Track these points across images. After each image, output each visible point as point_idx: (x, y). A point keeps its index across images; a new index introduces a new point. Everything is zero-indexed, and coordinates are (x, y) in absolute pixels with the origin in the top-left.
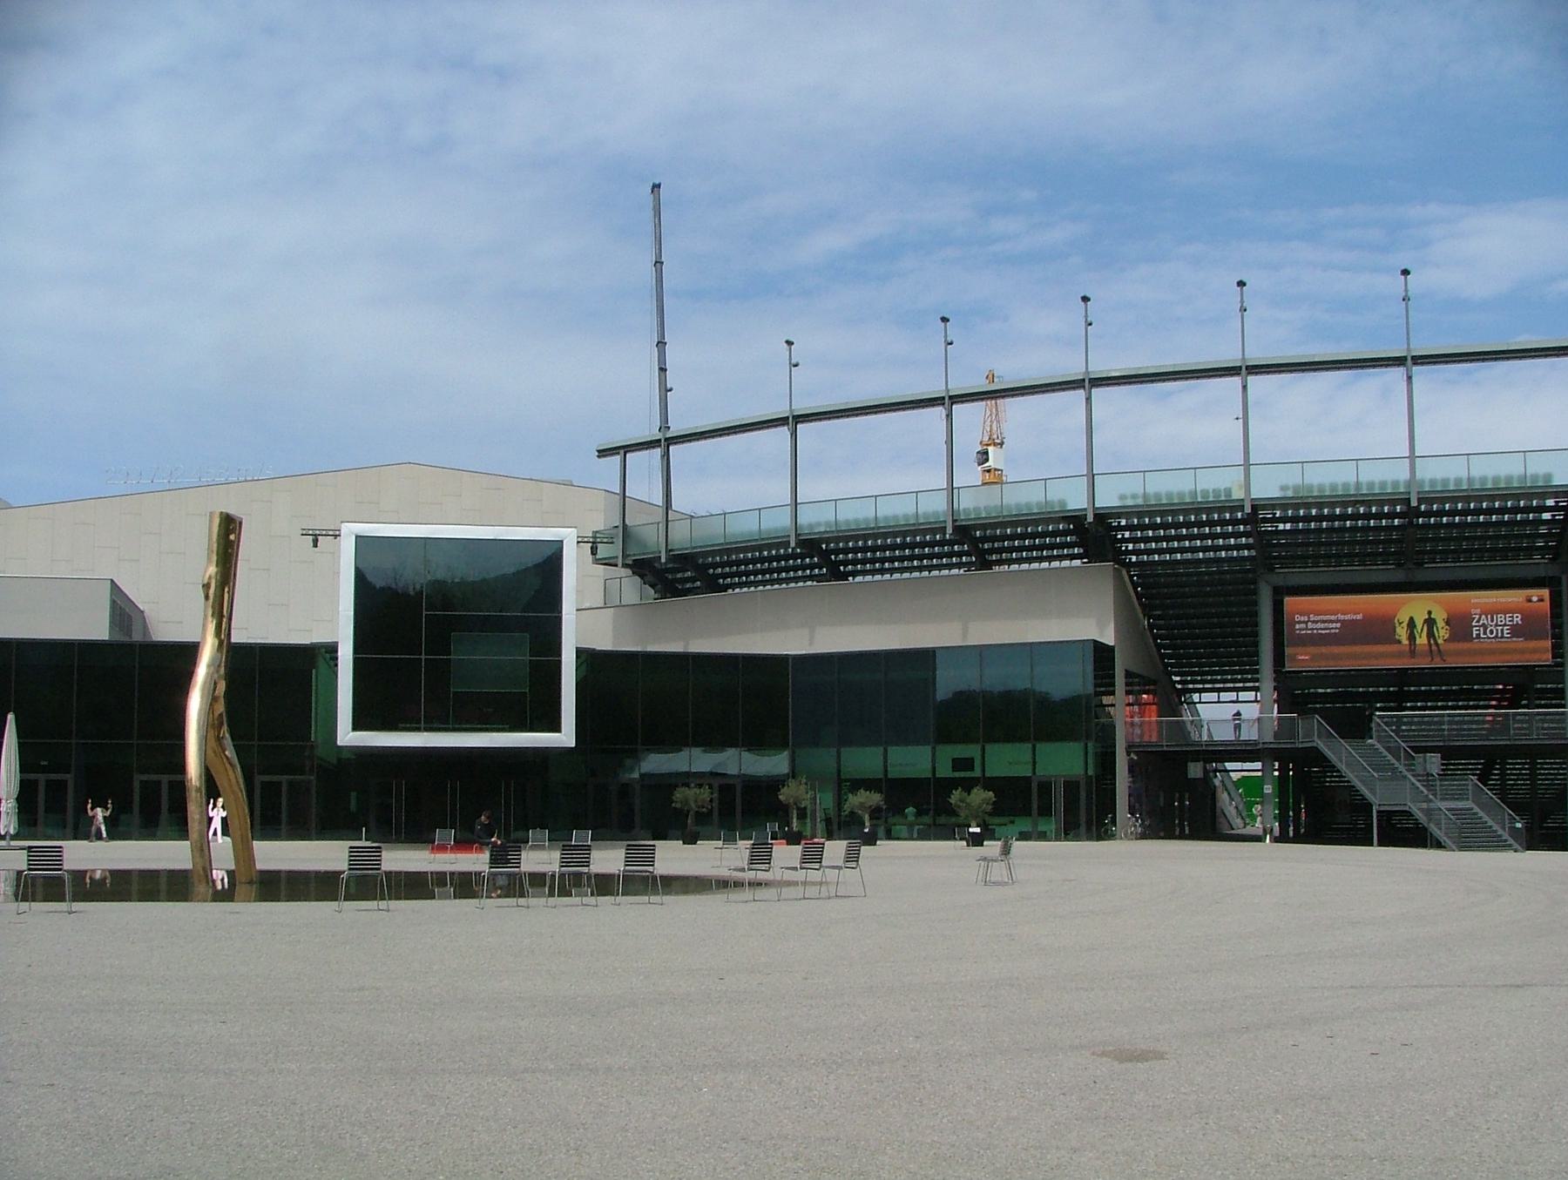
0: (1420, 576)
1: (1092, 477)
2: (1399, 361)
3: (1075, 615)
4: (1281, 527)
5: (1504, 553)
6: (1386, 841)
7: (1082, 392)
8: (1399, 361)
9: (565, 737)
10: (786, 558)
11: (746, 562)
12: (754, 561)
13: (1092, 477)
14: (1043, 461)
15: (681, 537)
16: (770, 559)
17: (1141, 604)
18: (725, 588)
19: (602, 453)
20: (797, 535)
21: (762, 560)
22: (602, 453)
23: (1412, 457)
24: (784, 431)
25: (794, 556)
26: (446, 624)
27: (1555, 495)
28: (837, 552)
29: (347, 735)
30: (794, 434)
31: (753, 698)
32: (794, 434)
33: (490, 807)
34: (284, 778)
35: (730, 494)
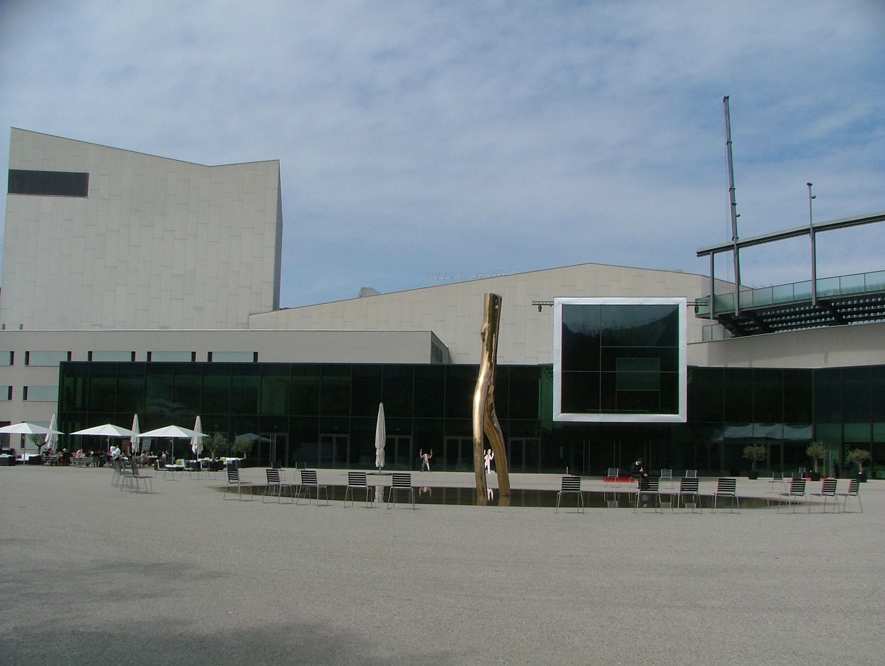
2: (805, 231)
7: (732, 251)
8: (805, 231)
9: (681, 417)
10: (810, 312)
11: (786, 315)
12: (791, 314)
15: (747, 301)
16: (800, 313)
18: (773, 330)
19: (701, 254)
20: (739, 309)
21: (795, 313)
22: (701, 254)
25: (815, 311)
28: (841, 307)
29: (558, 416)
30: (813, 239)
31: (792, 394)
32: (813, 239)
34: (523, 439)
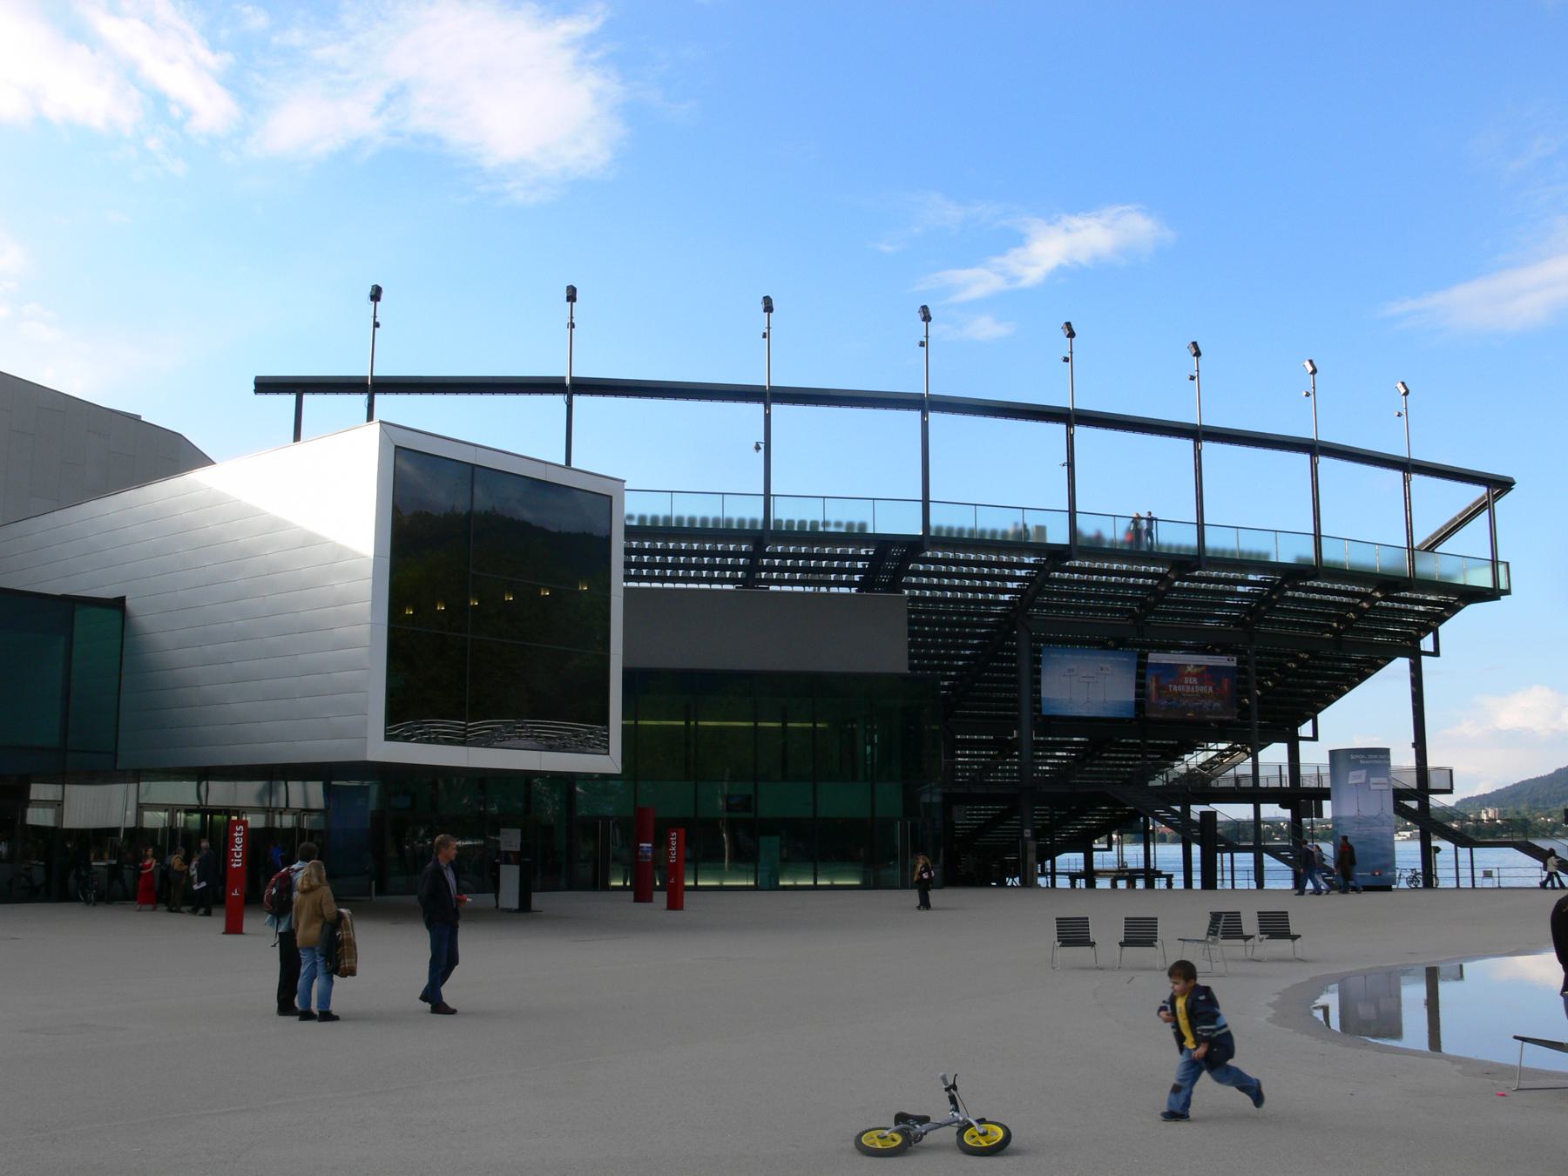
4: (1240, 589)
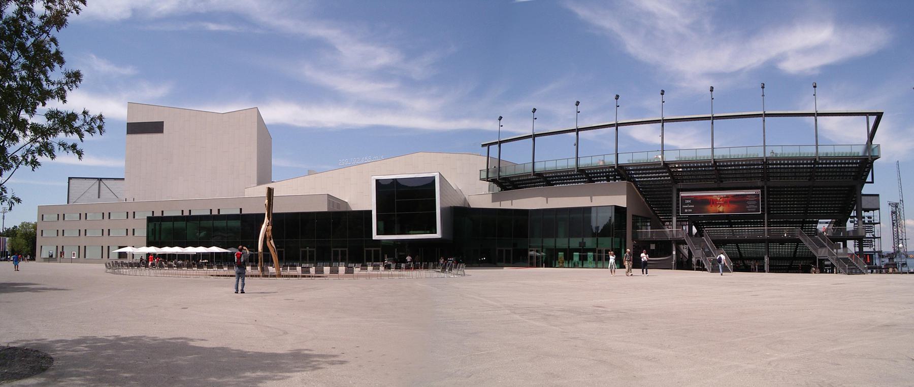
0: (722, 185)
1: (765, 146)
3: (611, 199)
5: (747, 178)
6: (773, 269)
8: (709, 118)
9: (375, 237)
13: (765, 146)
14: (598, 152)
17: (641, 192)
18: (553, 185)
22: (483, 145)
23: (713, 148)
24: (531, 140)
26: (405, 201)
27: (678, 164)
33: (426, 256)
35: (518, 159)
